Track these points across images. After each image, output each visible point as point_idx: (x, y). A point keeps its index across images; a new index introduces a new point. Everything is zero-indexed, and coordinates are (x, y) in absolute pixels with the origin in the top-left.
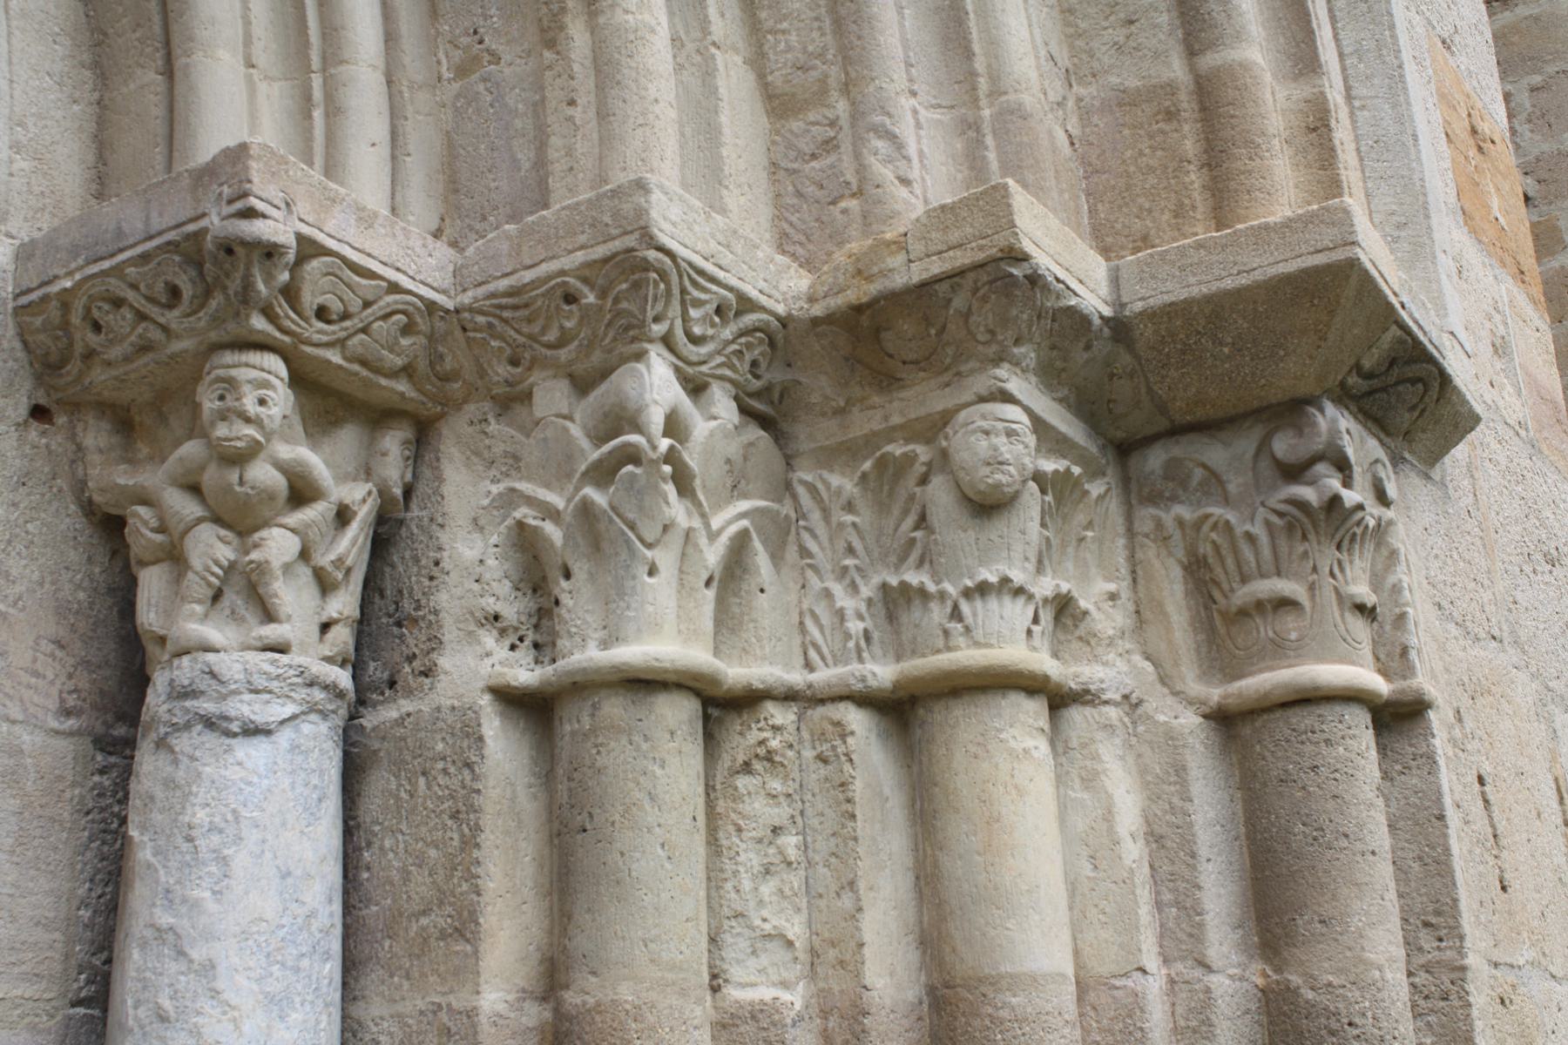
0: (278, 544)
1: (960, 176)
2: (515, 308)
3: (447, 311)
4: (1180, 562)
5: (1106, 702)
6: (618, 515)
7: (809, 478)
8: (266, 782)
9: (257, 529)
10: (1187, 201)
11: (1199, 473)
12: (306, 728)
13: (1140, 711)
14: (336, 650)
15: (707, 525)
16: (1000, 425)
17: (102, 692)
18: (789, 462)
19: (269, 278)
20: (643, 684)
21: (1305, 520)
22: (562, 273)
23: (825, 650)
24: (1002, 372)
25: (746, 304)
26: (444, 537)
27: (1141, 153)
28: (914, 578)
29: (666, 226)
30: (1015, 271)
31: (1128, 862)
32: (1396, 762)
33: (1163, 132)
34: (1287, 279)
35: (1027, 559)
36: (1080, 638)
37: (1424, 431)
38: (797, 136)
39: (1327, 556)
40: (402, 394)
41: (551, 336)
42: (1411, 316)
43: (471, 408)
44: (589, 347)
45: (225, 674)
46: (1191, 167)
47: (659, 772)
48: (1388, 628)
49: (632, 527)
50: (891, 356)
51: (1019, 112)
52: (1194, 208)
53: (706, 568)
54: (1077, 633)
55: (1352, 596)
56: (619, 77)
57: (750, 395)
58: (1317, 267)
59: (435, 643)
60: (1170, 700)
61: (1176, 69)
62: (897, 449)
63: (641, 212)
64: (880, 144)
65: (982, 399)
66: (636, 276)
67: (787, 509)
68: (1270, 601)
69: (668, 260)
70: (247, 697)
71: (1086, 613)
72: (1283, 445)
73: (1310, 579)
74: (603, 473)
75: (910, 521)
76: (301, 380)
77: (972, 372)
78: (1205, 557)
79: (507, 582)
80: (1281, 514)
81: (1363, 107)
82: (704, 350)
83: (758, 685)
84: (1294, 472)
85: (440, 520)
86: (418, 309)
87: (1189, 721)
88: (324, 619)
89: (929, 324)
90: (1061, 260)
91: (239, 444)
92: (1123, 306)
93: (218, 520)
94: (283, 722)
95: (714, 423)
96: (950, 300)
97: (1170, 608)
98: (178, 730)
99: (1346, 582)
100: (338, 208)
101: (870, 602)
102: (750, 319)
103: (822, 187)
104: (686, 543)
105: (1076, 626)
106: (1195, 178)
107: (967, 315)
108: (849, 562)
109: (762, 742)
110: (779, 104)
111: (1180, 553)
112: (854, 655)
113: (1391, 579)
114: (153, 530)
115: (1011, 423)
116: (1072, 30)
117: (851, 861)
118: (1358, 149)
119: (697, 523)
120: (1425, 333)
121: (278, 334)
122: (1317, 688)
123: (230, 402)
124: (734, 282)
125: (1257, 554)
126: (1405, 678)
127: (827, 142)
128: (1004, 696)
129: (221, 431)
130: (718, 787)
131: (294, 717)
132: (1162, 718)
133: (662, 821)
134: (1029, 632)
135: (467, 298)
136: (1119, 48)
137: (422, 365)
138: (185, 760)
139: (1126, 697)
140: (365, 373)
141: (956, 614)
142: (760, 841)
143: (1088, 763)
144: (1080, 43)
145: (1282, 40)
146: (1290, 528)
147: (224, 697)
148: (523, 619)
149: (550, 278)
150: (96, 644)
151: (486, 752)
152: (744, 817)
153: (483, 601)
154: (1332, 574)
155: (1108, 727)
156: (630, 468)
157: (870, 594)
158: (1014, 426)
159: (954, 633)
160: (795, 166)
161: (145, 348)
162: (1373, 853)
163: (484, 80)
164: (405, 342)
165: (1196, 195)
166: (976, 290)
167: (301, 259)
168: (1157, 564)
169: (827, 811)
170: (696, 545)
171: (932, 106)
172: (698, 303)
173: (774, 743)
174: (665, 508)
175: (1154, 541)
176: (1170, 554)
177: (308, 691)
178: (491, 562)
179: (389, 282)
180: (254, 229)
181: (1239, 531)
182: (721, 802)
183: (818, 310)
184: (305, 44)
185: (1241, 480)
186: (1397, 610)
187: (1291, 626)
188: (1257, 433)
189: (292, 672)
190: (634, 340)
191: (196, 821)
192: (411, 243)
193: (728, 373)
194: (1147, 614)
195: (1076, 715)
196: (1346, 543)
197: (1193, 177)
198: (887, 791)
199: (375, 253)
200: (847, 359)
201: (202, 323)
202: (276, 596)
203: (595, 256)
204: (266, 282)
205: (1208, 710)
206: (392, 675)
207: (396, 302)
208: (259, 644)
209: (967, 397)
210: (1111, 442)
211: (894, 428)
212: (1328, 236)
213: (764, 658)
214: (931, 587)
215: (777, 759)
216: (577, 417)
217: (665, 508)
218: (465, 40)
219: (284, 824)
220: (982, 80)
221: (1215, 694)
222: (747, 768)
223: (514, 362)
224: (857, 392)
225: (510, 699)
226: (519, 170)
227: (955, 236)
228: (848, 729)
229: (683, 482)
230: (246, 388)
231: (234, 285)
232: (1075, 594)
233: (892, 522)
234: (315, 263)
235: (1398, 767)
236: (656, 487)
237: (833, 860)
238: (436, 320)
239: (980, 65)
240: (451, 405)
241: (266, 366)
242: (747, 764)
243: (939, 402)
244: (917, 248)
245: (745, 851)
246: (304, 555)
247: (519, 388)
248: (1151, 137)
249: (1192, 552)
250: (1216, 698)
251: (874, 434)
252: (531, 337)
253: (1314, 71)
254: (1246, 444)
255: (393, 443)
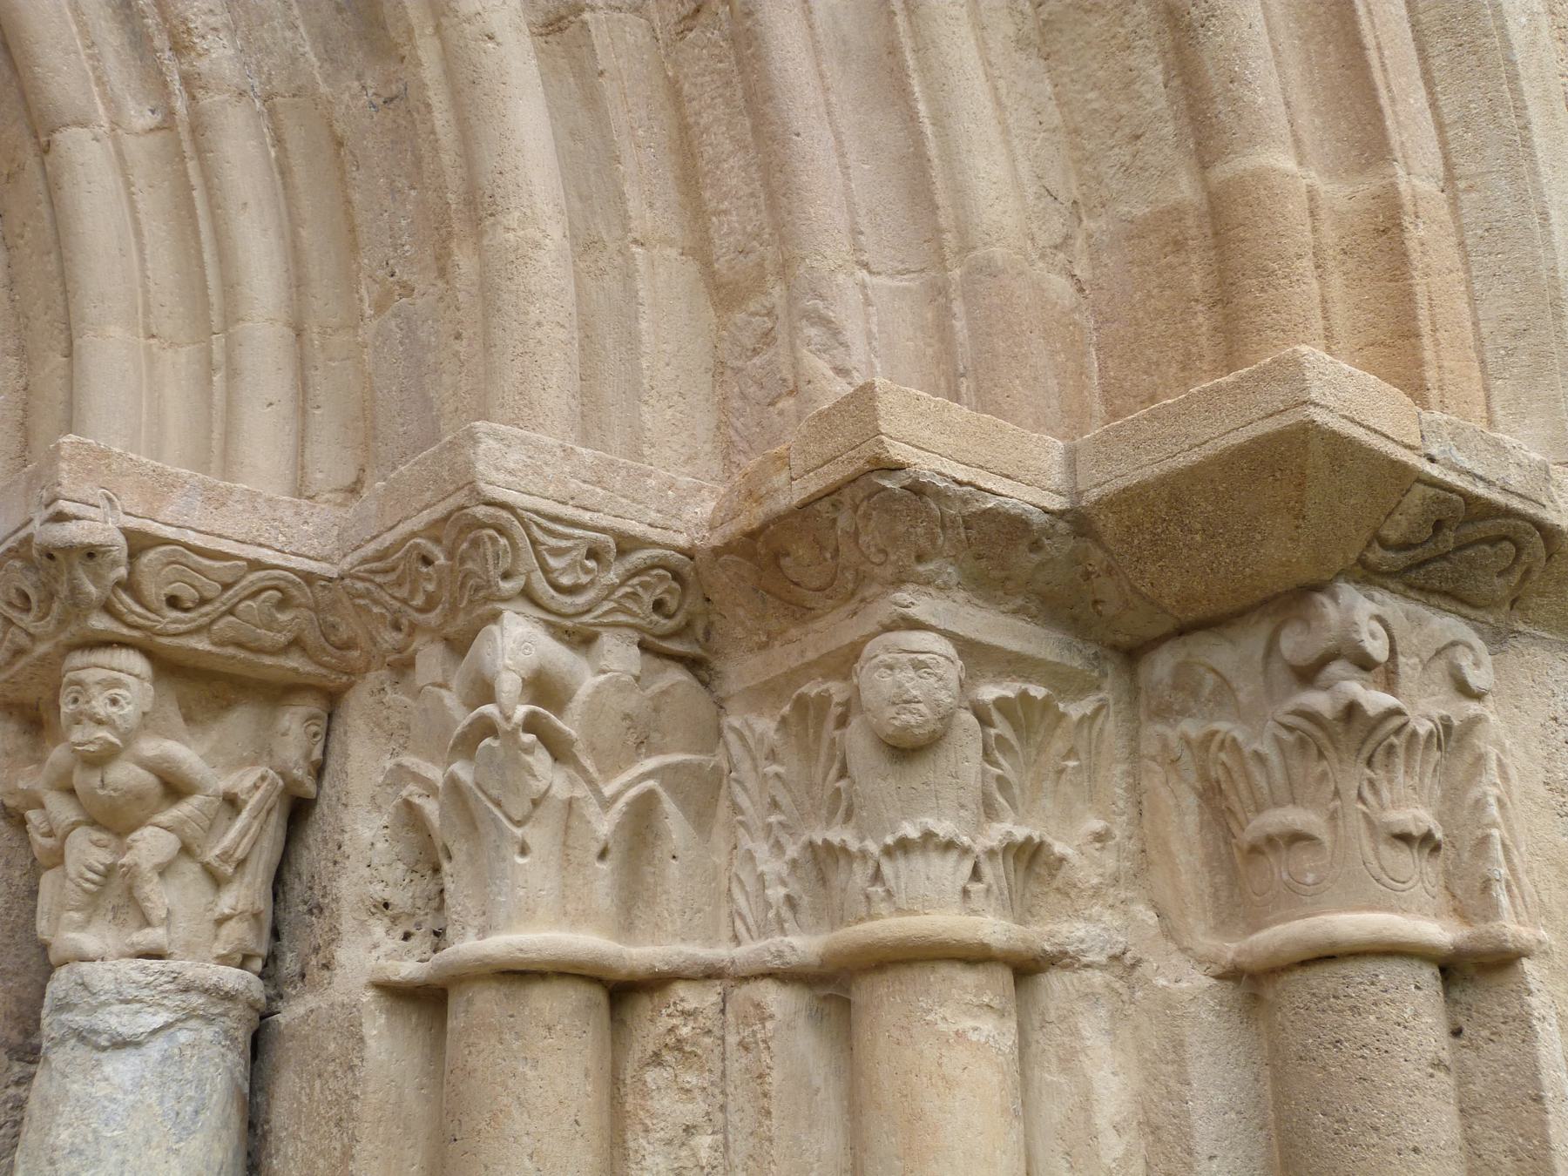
0: (151, 843)
1: (930, 351)
2: (385, 572)
3: (330, 580)
4: (1194, 788)
5: (1087, 966)
6: (484, 792)
7: (737, 723)
8: (131, 1097)
9: (133, 829)
10: (1194, 350)
11: (1210, 679)
12: (183, 1037)
13: (1138, 972)
14: (229, 948)
15: (597, 792)
16: (905, 657)
17: (19, 1000)
18: (720, 705)
19: (97, 579)
20: (518, 975)
21: (1319, 734)
22: (414, 534)
23: (750, 920)
24: (903, 596)
25: (626, 544)
26: (347, 818)
27: (1149, 296)
28: (838, 835)
29: (500, 477)
30: (888, 484)
31: (1107, 1161)
32: (1483, 1025)
33: (1170, 266)
34: (1241, 452)
35: (962, 806)
36: (1058, 889)
37: (1541, 595)
38: (740, 329)
39: (1353, 775)
40: (295, 670)
41: (419, 601)
42: (1453, 467)
43: (371, 676)
44: (453, 609)
45: (97, 985)
46: (1200, 307)
47: (530, 1074)
48: (1466, 855)
49: (498, 804)
50: (797, 584)
51: (988, 270)
52: (1201, 357)
53: (597, 840)
54: (1055, 884)
55: (1388, 825)
56: (499, 303)
57: (664, 637)
58: (1267, 434)
59: (334, 936)
60: (1176, 959)
61: (1185, 189)
62: (812, 689)
63: (470, 465)
64: (812, 332)
65: (887, 629)
66: (471, 536)
67: (720, 759)
68: (1281, 836)
69: (505, 514)
70: (116, 1008)
71: (1062, 860)
72: (1295, 644)
73: (1331, 806)
74: (467, 744)
75: (833, 772)
76: (169, 667)
77: (877, 596)
78: (1218, 782)
79: (401, 865)
80: (1290, 729)
81: (1470, 188)
82: (581, 600)
83: (661, 966)
84: (1307, 675)
85: (344, 800)
86: (293, 582)
87: (1198, 980)
88: (216, 915)
89: (822, 548)
90: (969, 458)
91: (92, 748)
92: (1080, 494)
93: (93, 823)
94: (155, 1032)
95: (602, 678)
96: (834, 521)
97: (1176, 846)
98: (56, 1045)
99: (1382, 807)
100: (179, 492)
101: (794, 863)
102: (639, 557)
103: (762, 387)
104: (569, 814)
105: (1053, 876)
106: (1202, 320)
107: (856, 535)
108: (773, 819)
109: (671, 1030)
110: (725, 293)
111: (1193, 778)
112: (775, 926)
113: (1474, 793)
114: (44, 835)
115: (926, 647)
116: (1078, 154)
117: (765, 1166)
118: (1461, 244)
119: (582, 791)
120: (1490, 484)
121: (125, 631)
122: (1334, 944)
123: (82, 706)
124: (604, 520)
125: (1269, 777)
126: (1486, 919)
127: (766, 334)
128: (933, 971)
129: (77, 735)
130: (628, 1081)
131: (167, 1026)
132: (1161, 982)
133: (532, 1129)
134: (965, 893)
135: (345, 565)
136: (1126, 169)
137: (312, 637)
138: (57, 1076)
139: (1115, 958)
140: (242, 654)
141: (877, 877)
142: (669, 1142)
143: (1066, 1039)
144: (1088, 168)
145: (1343, 125)
146: (1302, 744)
147: (94, 1009)
148: (419, 903)
149: (405, 540)
150: (13, 951)
151: (367, 1054)
152: (652, 1116)
153: (371, 888)
154: (1361, 797)
155: (1091, 997)
156: (487, 741)
157: (795, 855)
158: (922, 657)
159: (875, 899)
160: (739, 363)
161: (19, 652)
162: (1416, 1150)
163: (396, 316)
164: (283, 617)
165: (1203, 341)
166: (856, 508)
167: (134, 554)
168: (1164, 792)
169: (747, 1106)
170: (582, 817)
171: (898, 273)
172: (557, 552)
173: (685, 1031)
174: (532, 782)
175: (1161, 765)
176: (1181, 779)
177: (183, 997)
178: (380, 845)
179: (248, 561)
180: (66, 533)
181: (1247, 750)
182: (630, 1099)
183: (716, 540)
184: (207, 305)
185: (1251, 687)
186: (1479, 833)
187: (1306, 865)
188: (1263, 631)
189: (163, 979)
190: (487, 600)
191: (59, 1143)
192: (278, 514)
193: (622, 618)
194: (1153, 854)
195: (1055, 984)
196: (1379, 758)
197: (1201, 318)
198: (818, 1081)
199: (229, 532)
200: (756, 590)
201: (51, 627)
202: (148, 899)
203: (436, 516)
204: (94, 582)
205: (1219, 971)
206: (303, 968)
207: (262, 579)
208: (132, 951)
209: (871, 627)
210: (1115, 647)
211: (809, 665)
212: (1278, 394)
213: (675, 935)
214: (854, 846)
215: (688, 1048)
216: (454, 684)
217: (532, 782)
218: (380, 273)
219: (148, 1142)
220: (948, 236)
221: (1231, 949)
222: (656, 1060)
223: (397, 627)
224: (774, 625)
225: (398, 994)
226: (431, 409)
227: (829, 448)
228: (768, 1012)
229: (559, 749)
230: (95, 690)
231: (63, 591)
232: (1049, 839)
233: (820, 770)
234: (152, 555)
235: (1485, 1033)
236: (516, 760)
237: (750, 1163)
238: (317, 590)
239: (945, 219)
240: (354, 673)
241: (114, 665)
242: (656, 1054)
243: (848, 633)
244: (798, 463)
245: (652, 1154)
246: (186, 850)
247: (405, 654)
248: (1160, 274)
249: (1204, 776)
250: (1230, 955)
251: (794, 671)
252: (405, 601)
253: (1383, 158)
254: (1253, 641)
255: (293, 727)
